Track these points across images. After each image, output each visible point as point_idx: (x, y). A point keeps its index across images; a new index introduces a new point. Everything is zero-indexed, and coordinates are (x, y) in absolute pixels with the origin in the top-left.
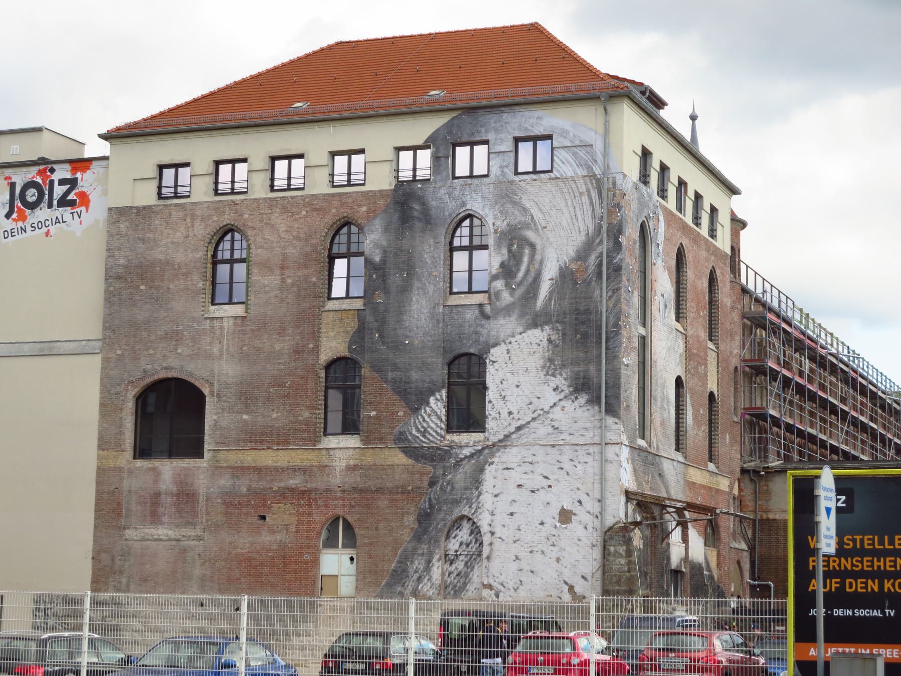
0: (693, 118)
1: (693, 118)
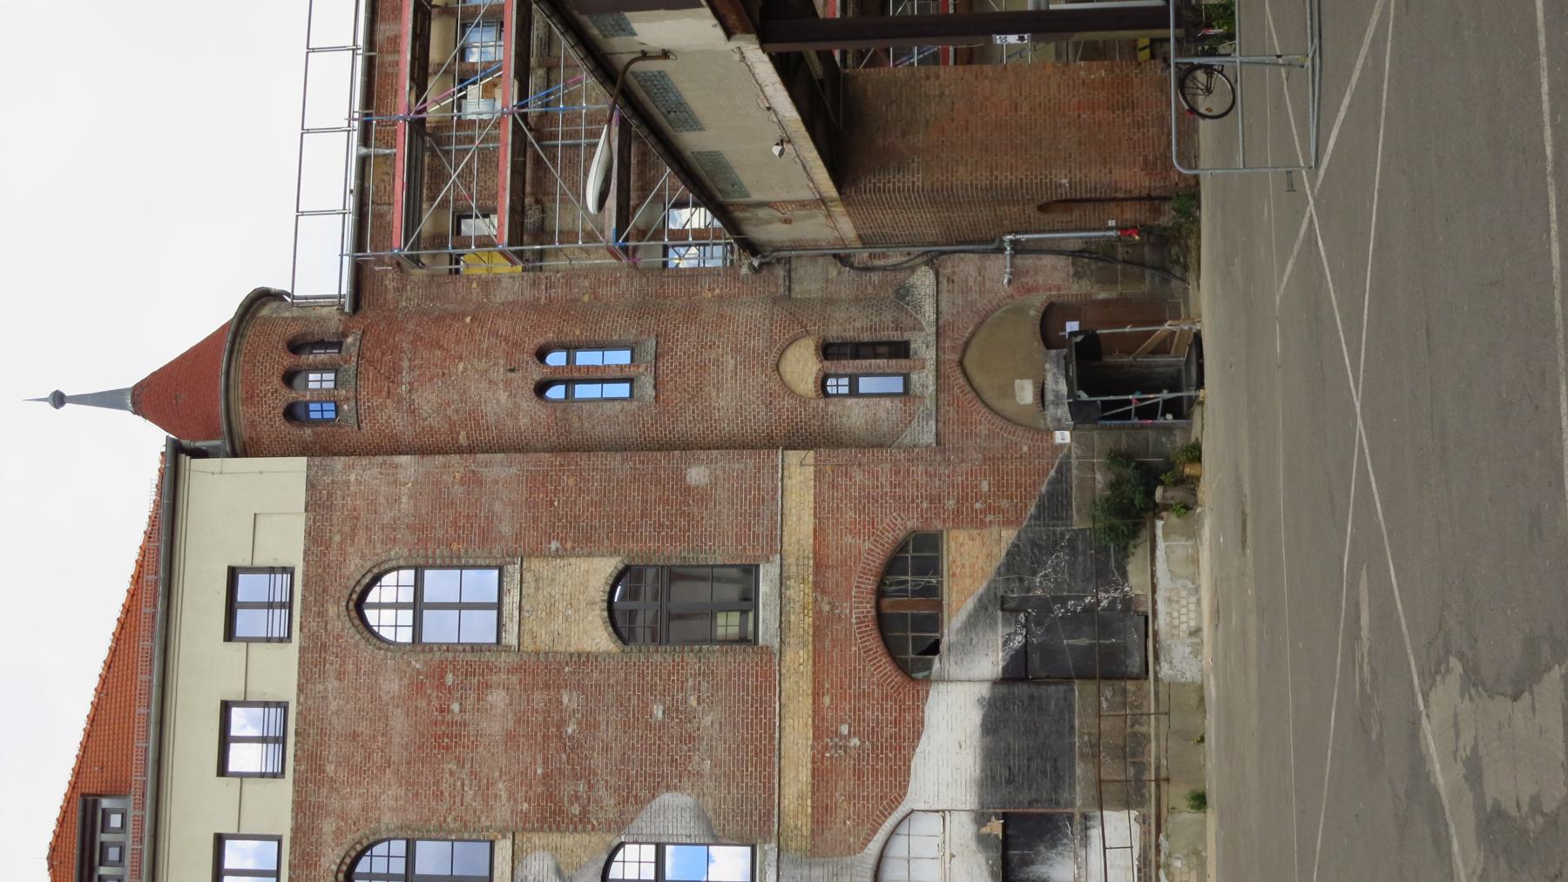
0: (59, 399)
1: (59, 399)
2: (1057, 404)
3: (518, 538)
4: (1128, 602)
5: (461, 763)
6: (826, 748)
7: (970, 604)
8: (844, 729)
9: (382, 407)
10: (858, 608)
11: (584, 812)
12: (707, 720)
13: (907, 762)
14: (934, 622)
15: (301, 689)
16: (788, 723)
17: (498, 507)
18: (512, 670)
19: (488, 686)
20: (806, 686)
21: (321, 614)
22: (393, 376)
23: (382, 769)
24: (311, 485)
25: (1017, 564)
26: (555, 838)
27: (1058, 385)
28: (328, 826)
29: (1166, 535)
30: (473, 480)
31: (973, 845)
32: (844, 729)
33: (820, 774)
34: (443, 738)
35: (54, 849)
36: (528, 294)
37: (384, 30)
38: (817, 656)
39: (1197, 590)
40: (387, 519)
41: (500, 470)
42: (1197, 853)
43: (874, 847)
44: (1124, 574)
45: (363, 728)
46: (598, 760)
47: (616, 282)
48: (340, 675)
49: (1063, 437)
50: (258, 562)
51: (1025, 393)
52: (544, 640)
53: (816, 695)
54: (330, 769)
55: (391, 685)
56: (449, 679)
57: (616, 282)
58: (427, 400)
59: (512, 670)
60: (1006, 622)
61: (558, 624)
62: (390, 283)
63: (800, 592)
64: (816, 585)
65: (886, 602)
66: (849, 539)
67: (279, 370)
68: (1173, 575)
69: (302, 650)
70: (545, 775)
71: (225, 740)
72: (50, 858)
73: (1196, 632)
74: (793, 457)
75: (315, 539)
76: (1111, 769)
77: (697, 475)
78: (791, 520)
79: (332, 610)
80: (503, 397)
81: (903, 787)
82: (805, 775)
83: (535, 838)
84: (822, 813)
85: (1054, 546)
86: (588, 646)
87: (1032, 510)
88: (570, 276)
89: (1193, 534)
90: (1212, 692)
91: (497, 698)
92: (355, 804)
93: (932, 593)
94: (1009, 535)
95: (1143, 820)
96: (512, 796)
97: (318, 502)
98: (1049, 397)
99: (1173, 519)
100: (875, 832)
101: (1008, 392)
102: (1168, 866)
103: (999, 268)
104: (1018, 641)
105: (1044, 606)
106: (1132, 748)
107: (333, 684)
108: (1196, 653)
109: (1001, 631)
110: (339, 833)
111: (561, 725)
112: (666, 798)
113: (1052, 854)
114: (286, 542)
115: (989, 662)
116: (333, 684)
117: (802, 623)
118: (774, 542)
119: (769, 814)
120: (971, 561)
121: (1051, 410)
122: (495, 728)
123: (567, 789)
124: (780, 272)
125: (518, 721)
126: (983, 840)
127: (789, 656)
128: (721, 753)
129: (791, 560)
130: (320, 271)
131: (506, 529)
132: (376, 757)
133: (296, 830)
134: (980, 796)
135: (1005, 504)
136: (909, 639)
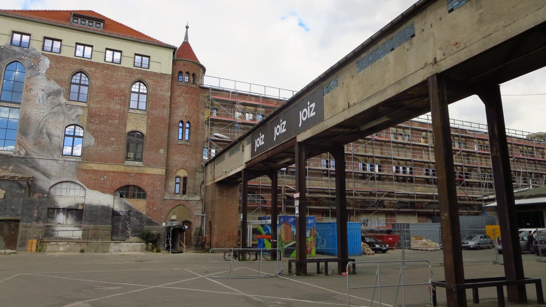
0: (187, 27)
1: (187, 27)
2: (171, 224)
3: (152, 114)
4: (128, 237)
5: (105, 98)
6: (101, 173)
7: (130, 204)
8: (105, 177)
9: (180, 90)
10: (131, 182)
11: (92, 122)
12: (110, 149)
13: (97, 190)
14: (127, 196)
15: (124, 67)
16: (108, 165)
17: (158, 111)
18: (124, 111)
19: (121, 105)
20: (115, 170)
21: (139, 73)
22: (186, 93)
23: (104, 82)
24: (166, 75)
25: (138, 214)
26: (87, 116)
27: (175, 224)
28: (93, 69)
29: (141, 245)
30: (164, 107)
31: (77, 203)
32: (105, 177)
33: (95, 172)
34: (111, 95)
35: (93, 12)
36: (200, 121)
37: (253, 98)
38: (121, 173)
39: (129, 251)
40: (157, 89)
41: (166, 112)
42: (70, 250)
43: (78, 182)
44: (134, 236)
45: (114, 79)
46: (103, 126)
47: (202, 138)
48: (126, 76)
49: (164, 224)
50: (151, 62)
51: (174, 217)
52: (130, 117)
53: (113, 172)
54: (106, 71)
55: (123, 86)
56: (123, 98)
57: (202, 138)
58: (181, 99)
59: (124, 111)
60: (126, 212)
61: (133, 121)
62: (205, 95)
63: (136, 170)
64: (137, 173)
65: (132, 187)
66: (146, 180)
67: (189, 71)
68: (133, 246)
69: (132, 69)
70: (100, 115)
71: (114, 51)
72: (91, 11)
73: (120, 251)
74: (164, 170)
75: (155, 74)
76: (91, 232)
77: (162, 151)
78: (151, 169)
79: (140, 76)
80: (181, 114)
81: (89, 188)
82: (96, 168)
83: (87, 112)
84: (87, 171)
85: (141, 222)
86: (128, 126)
87: (149, 218)
88: (203, 129)
89: (141, 251)
90: (106, 254)
91: (118, 107)
92: (97, 75)
93: (133, 197)
94: (144, 213)
95: (79, 239)
96: (96, 108)
97: (162, 76)
98: (172, 222)
99: (145, 247)
100: (82, 182)
101: (174, 214)
102: (68, 244)
103: (199, 213)
104: (121, 214)
105: (129, 220)
106: (96, 237)
107: (124, 74)
108: (115, 251)
109: (124, 210)
110: (91, 71)
111: (111, 119)
112: (93, 139)
113: (73, 219)
114: (154, 68)
115: (117, 207)
116: (124, 74)
117: (129, 170)
118: (147, 165)
119: (88, 160)
120: (139, 205)
121: (170, 222)
122: (112, 106)
123: (97, 119)
124: (201, 170)
125: (113, 111)
126: (78, 205)
127: (123, 167)
128: (102, 151)
129: (142, 168)
130: (208, 81)
131: (154, 112)
132: (107, 81)
133: (93, 63)
134: (88, 205)
135: (151, 212)
136: (125, 191)
